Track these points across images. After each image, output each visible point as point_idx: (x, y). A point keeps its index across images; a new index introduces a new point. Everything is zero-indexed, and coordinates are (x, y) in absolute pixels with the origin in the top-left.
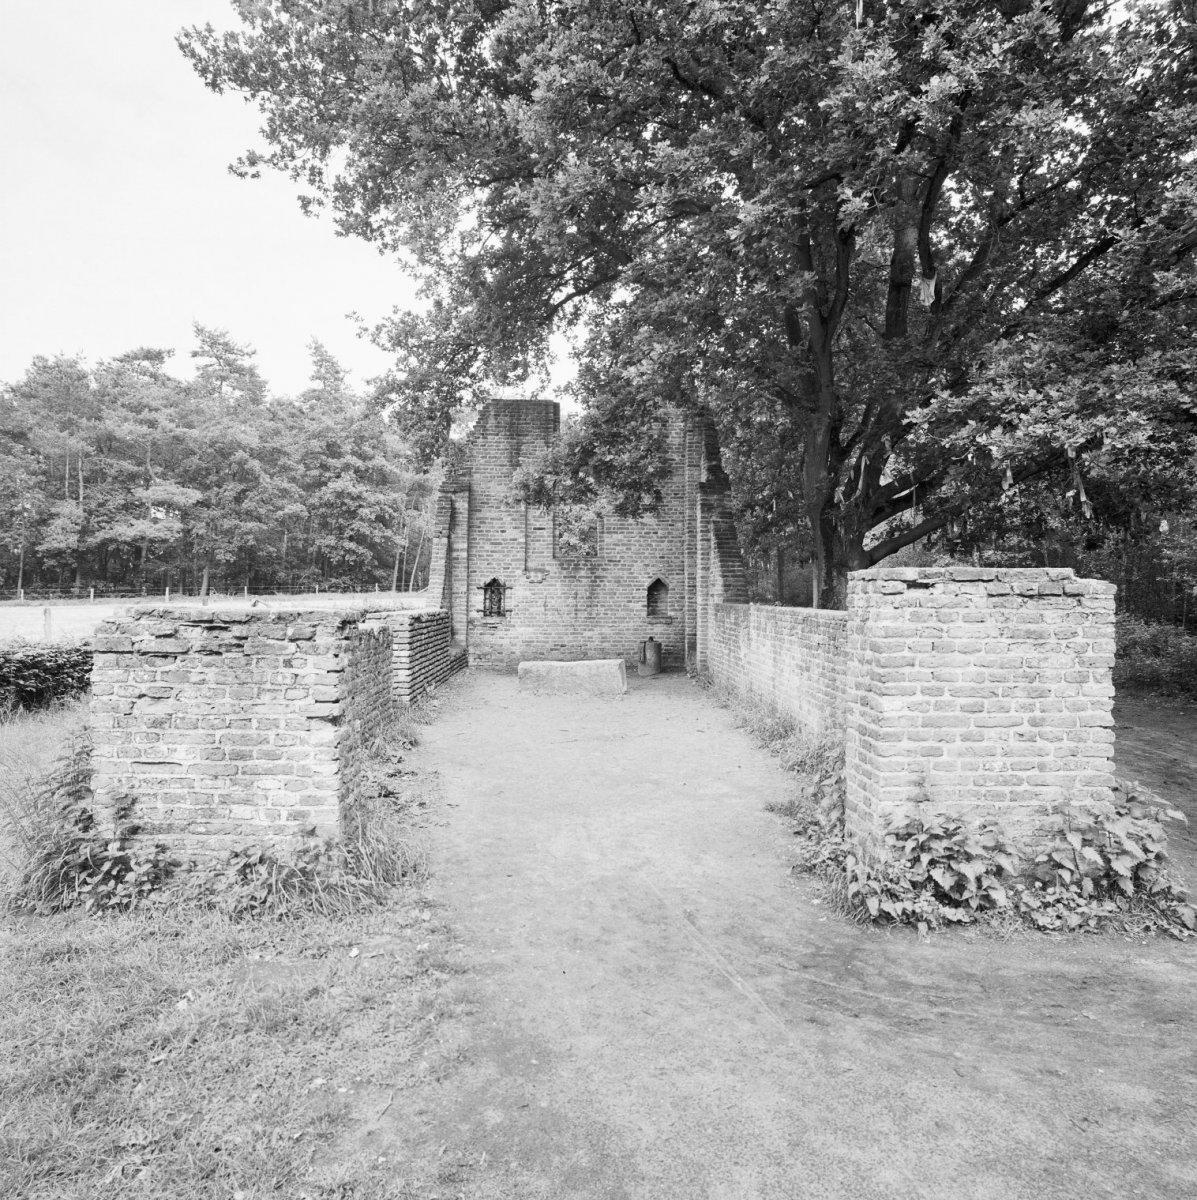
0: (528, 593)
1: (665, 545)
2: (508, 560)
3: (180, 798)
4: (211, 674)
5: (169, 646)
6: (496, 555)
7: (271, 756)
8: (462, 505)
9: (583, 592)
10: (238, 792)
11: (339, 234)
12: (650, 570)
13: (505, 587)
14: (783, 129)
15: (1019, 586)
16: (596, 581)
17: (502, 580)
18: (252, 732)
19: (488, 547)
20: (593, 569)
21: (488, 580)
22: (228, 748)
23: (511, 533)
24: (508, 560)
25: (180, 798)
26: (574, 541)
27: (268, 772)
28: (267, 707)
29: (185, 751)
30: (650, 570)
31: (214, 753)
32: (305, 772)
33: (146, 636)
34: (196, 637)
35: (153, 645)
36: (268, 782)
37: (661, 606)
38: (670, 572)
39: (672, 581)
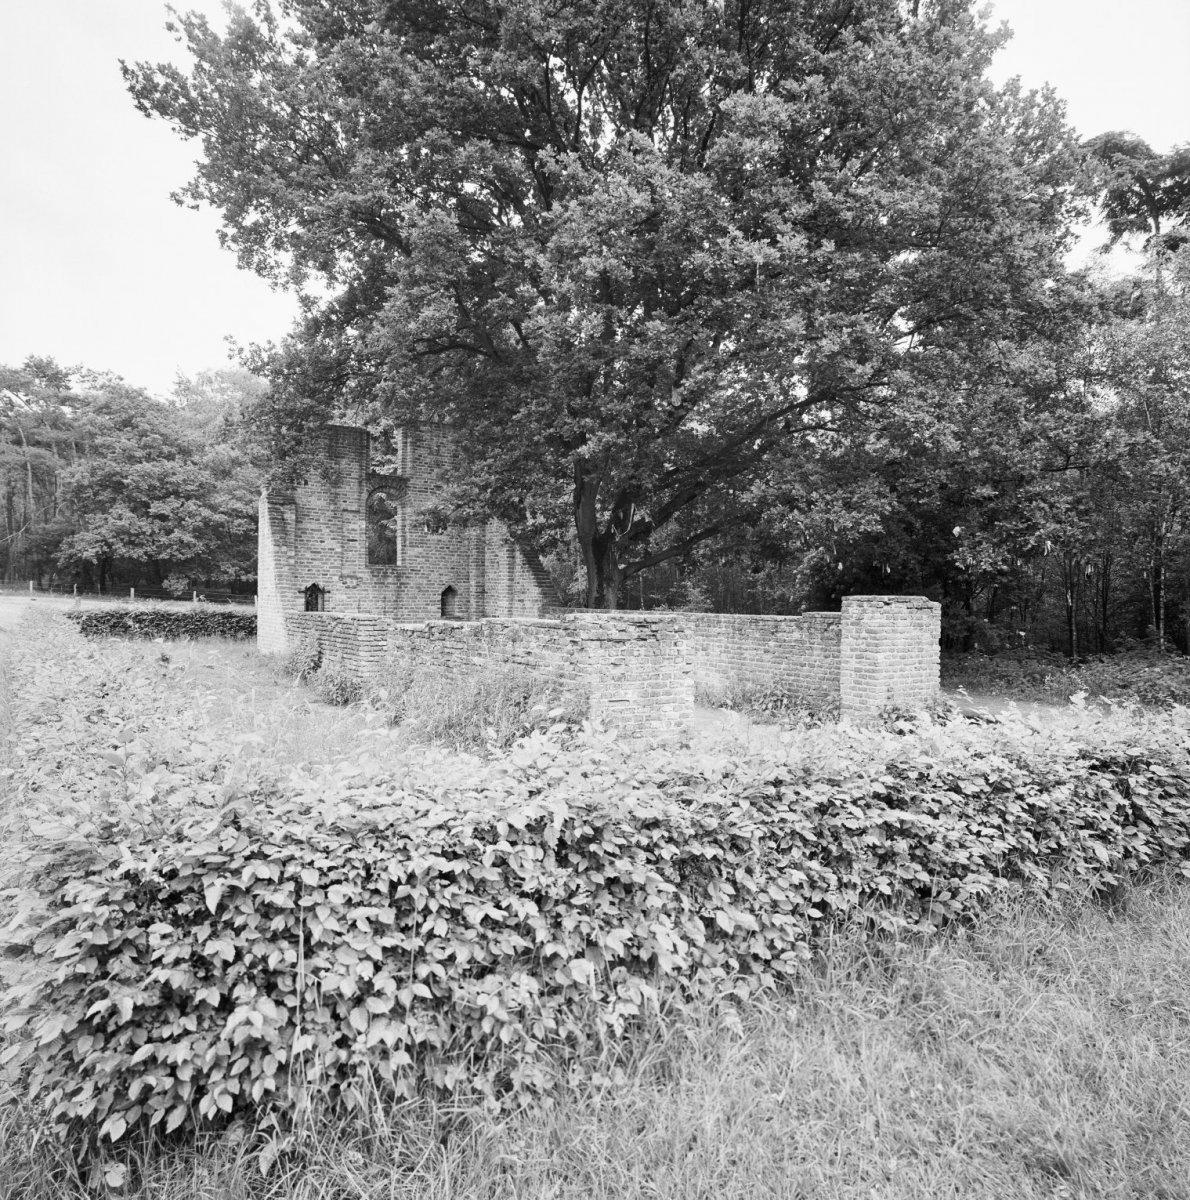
0: (344, 597)
1: (455, 558)
2: (327, 567)
3: (629, 720)
4: (643, 651)
5: (624, 636)
6: (316, 563)
7: (668, 693)
8: (290, 516)
9: (390, 595)
10: (654, 714)
11: (240, 267)
12: (444, 578)
13: (323, 592)
14: (344, 144)
15: (916, 604)
16: (400, 586)
17: (321, 585)
18: (660, 681)
19: (308, 555)
20: (398, 577)
21: (309, 585)
22: (650, 690)
23: (329, 543)
24: (327, 567)
25: (629, 720)
26: (188, 538)
27: (668, 702)
28: (667, 668)
29: (631, 693)
30: (444, 578)
31: (645, 695)
32: (683, 701)
33: (614, 631)
34: (634, 631)
35: (616, 635)
36: (667, 707)
37: (449, 608)
38: (458, 580)
39: (460, 587)
